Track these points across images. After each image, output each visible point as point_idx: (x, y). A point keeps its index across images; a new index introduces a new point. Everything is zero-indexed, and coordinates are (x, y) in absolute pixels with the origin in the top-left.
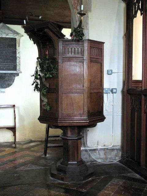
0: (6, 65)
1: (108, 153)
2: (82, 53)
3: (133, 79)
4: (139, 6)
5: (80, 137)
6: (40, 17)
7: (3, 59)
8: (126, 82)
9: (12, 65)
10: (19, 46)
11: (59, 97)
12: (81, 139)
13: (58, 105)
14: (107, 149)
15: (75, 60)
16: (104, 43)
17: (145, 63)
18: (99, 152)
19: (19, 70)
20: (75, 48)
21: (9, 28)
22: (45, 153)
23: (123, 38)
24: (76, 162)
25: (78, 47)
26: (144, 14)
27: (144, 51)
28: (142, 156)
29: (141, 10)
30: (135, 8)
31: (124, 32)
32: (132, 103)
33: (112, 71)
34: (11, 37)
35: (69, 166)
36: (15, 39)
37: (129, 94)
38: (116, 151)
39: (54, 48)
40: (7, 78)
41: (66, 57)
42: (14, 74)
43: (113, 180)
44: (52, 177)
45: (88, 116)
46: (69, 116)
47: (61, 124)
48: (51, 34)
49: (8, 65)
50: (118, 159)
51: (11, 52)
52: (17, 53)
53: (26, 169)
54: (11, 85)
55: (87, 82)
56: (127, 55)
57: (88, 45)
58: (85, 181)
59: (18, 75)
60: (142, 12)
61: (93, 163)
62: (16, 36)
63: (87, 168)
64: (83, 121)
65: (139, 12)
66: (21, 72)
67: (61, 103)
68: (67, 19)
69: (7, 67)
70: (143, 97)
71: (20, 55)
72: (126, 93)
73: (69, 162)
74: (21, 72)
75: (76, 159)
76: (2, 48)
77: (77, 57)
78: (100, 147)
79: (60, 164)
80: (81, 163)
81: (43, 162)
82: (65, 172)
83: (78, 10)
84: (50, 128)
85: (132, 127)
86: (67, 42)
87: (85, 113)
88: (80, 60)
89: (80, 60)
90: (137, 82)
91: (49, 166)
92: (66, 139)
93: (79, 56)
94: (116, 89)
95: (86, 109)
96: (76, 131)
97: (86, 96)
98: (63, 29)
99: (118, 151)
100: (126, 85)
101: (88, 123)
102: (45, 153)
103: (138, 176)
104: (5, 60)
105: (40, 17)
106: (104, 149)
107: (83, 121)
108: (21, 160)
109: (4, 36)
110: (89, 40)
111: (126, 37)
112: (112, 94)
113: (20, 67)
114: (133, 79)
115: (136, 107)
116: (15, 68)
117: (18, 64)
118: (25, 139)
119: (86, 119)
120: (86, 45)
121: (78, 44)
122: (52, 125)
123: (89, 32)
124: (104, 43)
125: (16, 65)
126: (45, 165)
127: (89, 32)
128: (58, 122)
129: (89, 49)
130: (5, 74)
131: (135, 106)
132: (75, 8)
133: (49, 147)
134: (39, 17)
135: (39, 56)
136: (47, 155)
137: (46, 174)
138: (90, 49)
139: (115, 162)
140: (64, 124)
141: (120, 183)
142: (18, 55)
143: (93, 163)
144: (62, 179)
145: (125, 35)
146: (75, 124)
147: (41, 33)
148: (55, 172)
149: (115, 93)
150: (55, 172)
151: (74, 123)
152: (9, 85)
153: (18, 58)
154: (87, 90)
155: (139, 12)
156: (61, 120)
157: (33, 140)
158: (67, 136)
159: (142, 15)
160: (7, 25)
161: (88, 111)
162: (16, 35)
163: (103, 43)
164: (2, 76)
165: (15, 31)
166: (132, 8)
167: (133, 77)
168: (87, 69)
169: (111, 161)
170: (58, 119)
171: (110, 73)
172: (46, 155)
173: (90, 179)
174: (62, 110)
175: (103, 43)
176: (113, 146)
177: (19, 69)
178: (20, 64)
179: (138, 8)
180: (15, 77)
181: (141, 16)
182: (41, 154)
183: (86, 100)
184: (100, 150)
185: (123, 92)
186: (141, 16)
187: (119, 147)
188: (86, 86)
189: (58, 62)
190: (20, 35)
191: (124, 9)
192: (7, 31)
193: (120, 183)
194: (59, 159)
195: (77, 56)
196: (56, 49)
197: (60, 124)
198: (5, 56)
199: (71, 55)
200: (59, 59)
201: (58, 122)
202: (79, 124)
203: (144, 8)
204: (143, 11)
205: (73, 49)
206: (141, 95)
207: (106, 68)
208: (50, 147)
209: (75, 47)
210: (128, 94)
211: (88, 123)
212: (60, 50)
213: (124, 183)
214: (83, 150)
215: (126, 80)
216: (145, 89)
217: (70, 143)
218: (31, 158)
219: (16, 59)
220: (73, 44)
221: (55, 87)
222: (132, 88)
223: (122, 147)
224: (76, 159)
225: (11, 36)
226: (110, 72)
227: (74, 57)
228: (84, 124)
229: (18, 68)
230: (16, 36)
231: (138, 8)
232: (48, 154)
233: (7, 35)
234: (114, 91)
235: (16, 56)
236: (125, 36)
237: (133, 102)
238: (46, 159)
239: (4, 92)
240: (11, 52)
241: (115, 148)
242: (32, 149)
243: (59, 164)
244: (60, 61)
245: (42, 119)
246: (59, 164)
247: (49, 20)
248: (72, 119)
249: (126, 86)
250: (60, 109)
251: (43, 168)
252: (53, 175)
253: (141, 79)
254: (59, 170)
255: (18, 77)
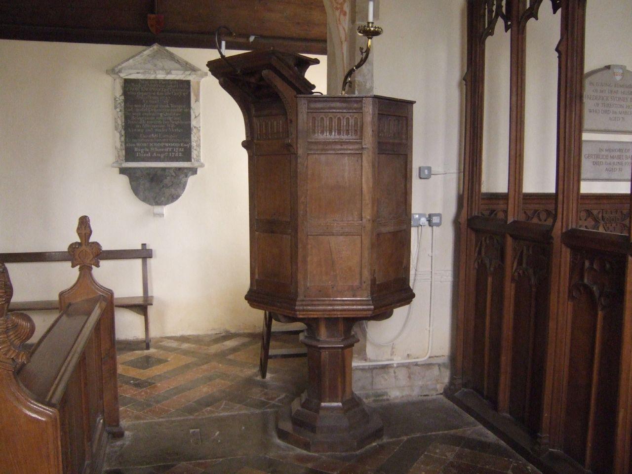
0: (165, 147)
1: (417, 374)
2: (359, 130)
3: (484, 189)
4: (499, 7)
5: (349, 341)
6: (252, 39)
7: (157, 133)
8: (466, 196)
9: (180, 147)
10: (197, 100)
11: (300, 246)
12: (352, 345)
13: (297, 264)
14: (416, 364)
15: (341, 149)
16: (415, 102)
17: (516, 154)
18: (395, 373)
19: (198, 161)
20: (339, 119)
21: (172, 57)
22: (263, 371)
23: (460, 84)
24: (340, 404)
25: (347, 115)
26: (515, 28)
27: (514, 124)
28: (502, 387)
29: (506, 18)
30: (491, 11)
31: (462, 71)
32: (480, 253)
33: (429, 169)
34: (177, 78)
35: (322, 413)
36: (188, 83)
37: (472, 229)
38: (437, 368)
39: (286, 113)
40: (167, 181)
41: (316, 143)
42: (185, 171)
43: (430, 447)
44: (280, 437)
45: (372, 293)
46: (324, 292)
47: (303, 315)
48: (279, 84)
49: (169, 147)
50: (440, 388)
51: (179, 116)
52: (193, 117)
53: (217, 414)
54: (178, 197)
55: (370, 206)
56: (468, 133)
57: (373, 110)
58: (363, 450)
59: (194, 171)
60: (509, 23)
61: (381, 398)
62: (190, 74)
63: (366, 416)
64: (359, 307)
65: (500, 23)
66: (202, 166)
67: (305, 262)
68: (315, 32)
69: (169, 152)
70: (509, 240)
71: (199, 122)
72: (464, 226)
73: (323, 404)
74: (202, 166)
75: (340, 393)
76: (157, 106)
77: (344, 142)
78: (397, 360)
79: (299, 408)
80: (353, 403)
81: (257, 394)
82: (313, 429)
83: (346, 12)
84: (274, 322)
85: (480, 313)
86: (319, 101)
87: (364, 285)
88: (352, 150)
89: (352, 150)
90: (494, 197)
91: (274, 406)
92: (316, 347)
93: (351, 137)
94: (439, 215)
95: (366, 274)
96: (341, 327)
97: (367, 242)
98: (310, 66)
99: (442, 369)
100: (465, 204)
101: (370, 312)
102: (263, 371)
103: (491, 437)
104: (164, 136)
105: (252, 39)
106: (407, 366)
107: (359, 307)
108: (205, 390)
109: (161, 76)
110: (376, 97)
111: (466, 85)
112: (431, 228)
113: (199, 152)
114: (484, 189)
115: (490, 264)
116: (187, 156)
117: (194, 144)
118: (214, 329)
119: (367, 301)
120: (369, 109)
121: (350, 108)
122: (281, 315)
123: (372, 69)
124: (415, 102)
125: (190, 147)
126: (263, 404)
127: (375, 71)
128: (296, 308)
129: (376, 119)
130: (164, 169)
131: (487, 262)
132: (337, 9)
133: (271, 357)
134: (248, 38)
135: (247, 137)
136: (268, 376)
137: (265, 429)
138: (379, 119)
139: (434, 395)
140: (310, 313)
141: (448, 454)
142: (194, 123)
143: (381, 398)
144: (306, 446)
145: (464, 79)
146: (339, 313)
147: (253, 80)
148: (287, 426)
149: (438, 225)
150: (287, 426)
151: (337, 310)
152: (174, 198)
153: (194, 131)
154: (369, 226)
155: (500, 23)
156: (304, 303)
157: (233, 331)
158: (319, 341)
159: (509, 31)
160: (167, 48)
161: (373, 281)
162: (189, 72)
163: (412, 103)
164: (156, 174)
165: (187, 63)
166: (482, 11)
167: (482, 186)
168: (370, 176)
169: (425, 394)
170: (295, 300)
171: (426, 174)
172: (264, 376)
173: (374, 444)
174: (305, 278)
175: (412, 103)
176: (430, 357)
177: (198, 156)
178: (199, 146)
179: (499, 13)
180: (187, 176)
181: (506, 31)
182: (252, 371)
183: (366, 254)
184: (397, 367)
185: (456, 222)
186: (506, 31)
187: (445, 360)
188: (368, 217)
189: (296, 154)
190: (199, 72)
191: (462, 14)
192: (169, 64)
193: (448, 454)
194: (298, 394)
195: (344, 137)
196: (291, 121)
197: (301, 313)
198: (163, 126)
199: (328, 136)
200: (299, 145)
201: (296, 308)
202: (348, 313)
203: (514, 13)
204: (510, 20)
205: (335, 121)
206: (504, 236)
207: (417, 162)
208: (275, 356)
209: (339, 115)
210: (469, 230)
211: (370, 312)
212: (300, 121)
213: (459, 456)
214: (357, 368)
215: (466, 193)
216: (514, 222)
217: (325, 355)
218: (229, 383)
219: (190, 133)
220: (334, 108)
221: (288, 220)
222: (480, 215)
223: (453, 358)
224: (340, 393)
225: (177, 75)
226: (426, 172)
227: (335, 143)
228: (360, 314)
229: (194, 154)
230: (190, 74)
231: (499, 13)
232: (271, 373)
233: (169, 73)
234: (435, 220)
235: (190, 125)
236: (464, 82)
237: (483, 250)
238: (264, 386)
239: (161, 215)
240: (179, 116)
241: (434, 361)
242: (231, 357)
243: (296, 406)
244: (300, 152)
245: (254, 298)
246: (296, 406)
247: (274, 47)
248: (330, 300)
249: (464, 211)
250: (300, 277)
251: (257, 411)
252: (282, 435)
253: (506, 191)
254: (299, 422)
255: (195, 176)
